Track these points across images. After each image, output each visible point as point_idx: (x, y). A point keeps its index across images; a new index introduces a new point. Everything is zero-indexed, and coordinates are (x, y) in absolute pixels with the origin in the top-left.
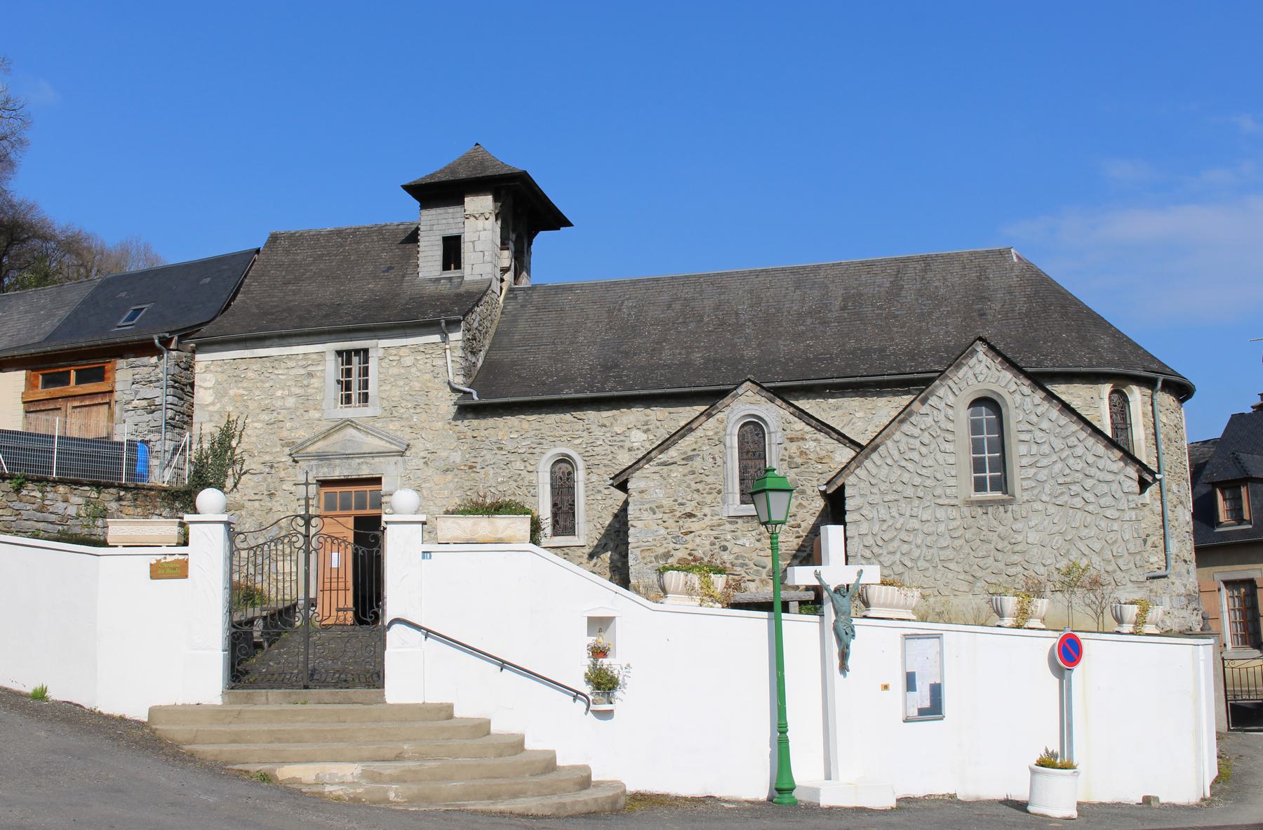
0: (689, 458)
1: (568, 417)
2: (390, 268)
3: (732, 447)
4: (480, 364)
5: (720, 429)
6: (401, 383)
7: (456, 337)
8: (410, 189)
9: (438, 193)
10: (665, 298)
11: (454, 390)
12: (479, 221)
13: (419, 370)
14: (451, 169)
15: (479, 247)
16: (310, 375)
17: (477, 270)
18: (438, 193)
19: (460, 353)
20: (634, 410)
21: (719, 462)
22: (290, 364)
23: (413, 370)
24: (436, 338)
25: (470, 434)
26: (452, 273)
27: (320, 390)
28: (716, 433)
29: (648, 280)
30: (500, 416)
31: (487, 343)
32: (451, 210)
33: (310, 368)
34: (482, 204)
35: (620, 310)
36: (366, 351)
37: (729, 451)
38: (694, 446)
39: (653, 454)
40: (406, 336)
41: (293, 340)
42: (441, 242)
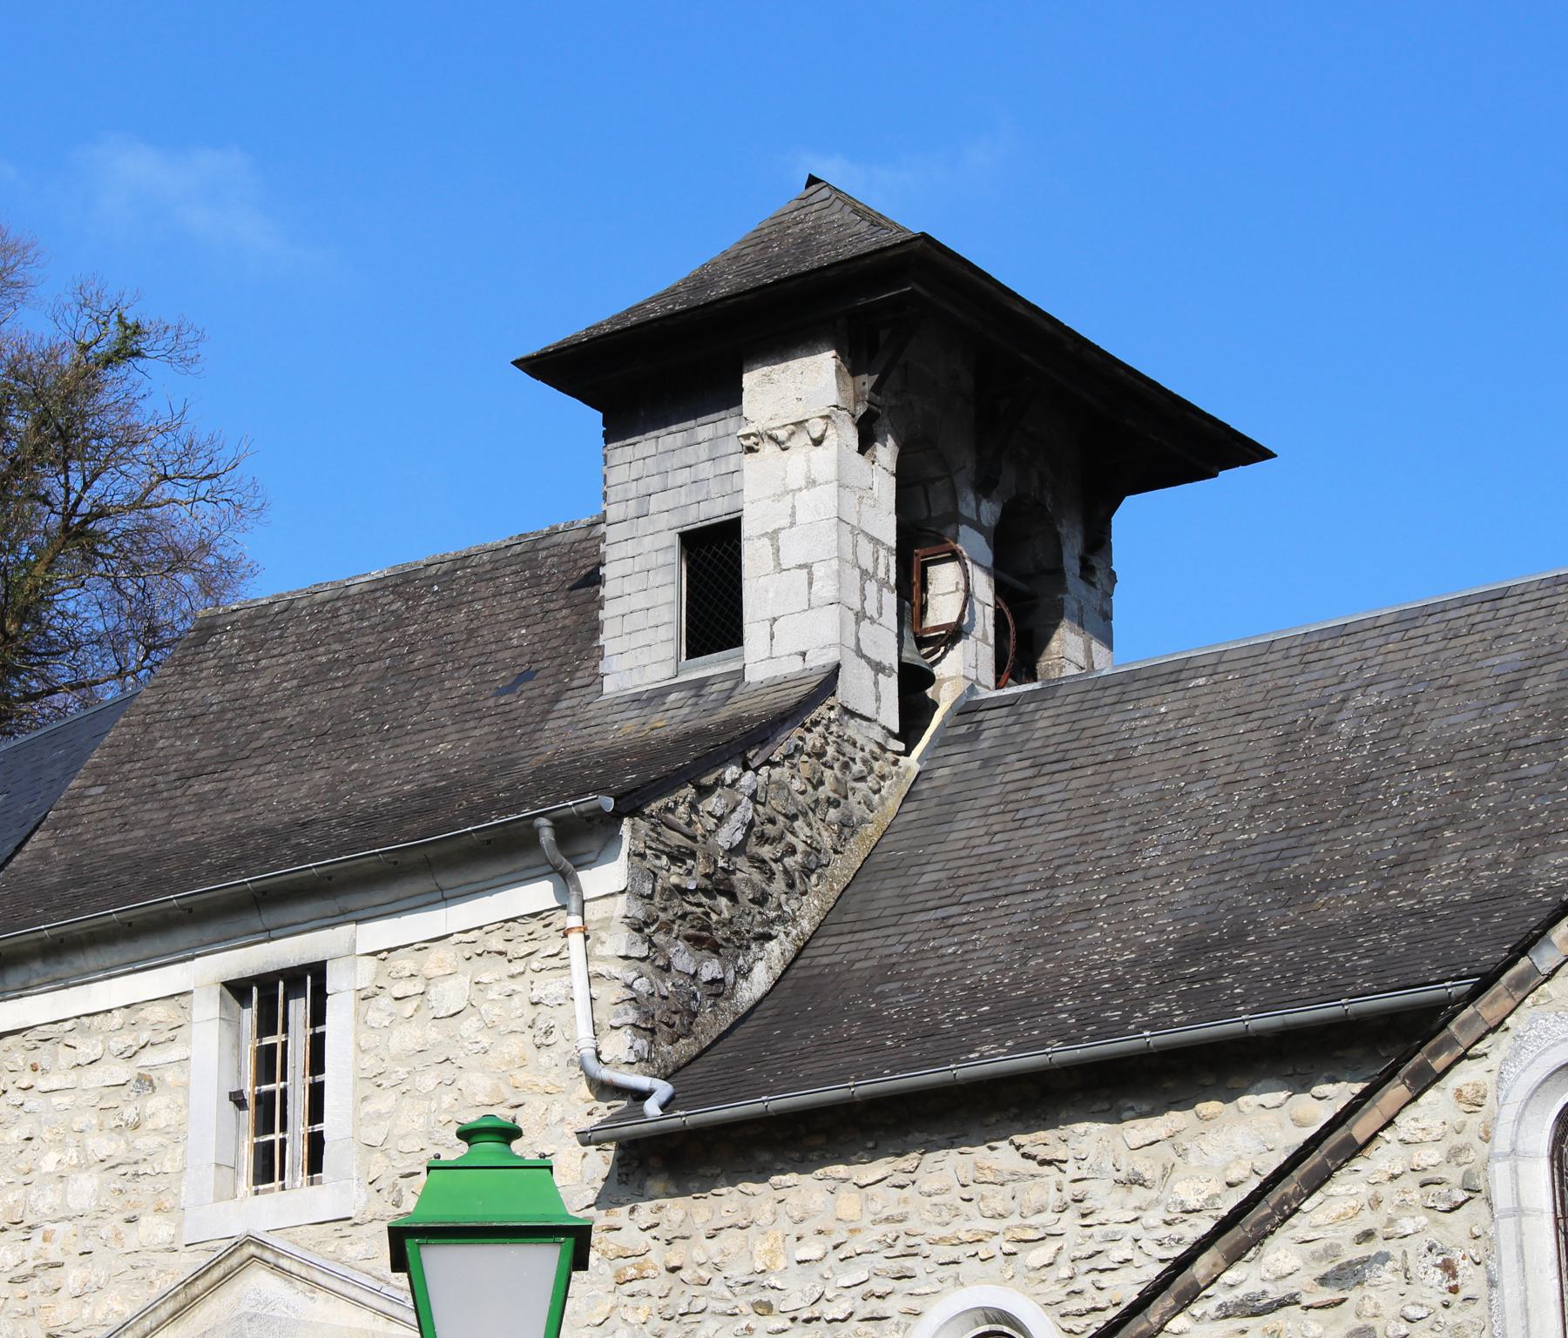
0: (1345, 1275)
1: (1002, 1156)
2: (527, 676)
3: (1519, 1211)
4: (760, 980)
5: (1470, 1137)
6: (428, 1081)
7: (606, 878)
8: (560, 367)
9: (654, 370)
10: (1511, 656)
11: (604, 1089)
12: (799, 462)
13: (490, 1027)
14: (698, 282)
15: (793, 553)
16: (146, 1083)
17: (789, 641)
18: (654, 370)
19: (618, 941)
20: (1248, 1101)
21: (1471, 1279)
22: (88, 1048)
23: (468, 1025)
24: (539, 894)
25: (660, 1256)
26: (712, 666)
27: (175, 1135)
28: (1455, 1154)
29: (1464, 602)
30: (761, 1174)
31: (809, 910)
32: (705, 429)
33: (147, 1058)
34: (800, 389)
35: (1324, 729)
36: (318, 970)
37: (1506, 1227)
38: (1369, 1220)
39: (1201, 1268)
40: (444, 898)
41: (90, 959)
42: (674, 555)
